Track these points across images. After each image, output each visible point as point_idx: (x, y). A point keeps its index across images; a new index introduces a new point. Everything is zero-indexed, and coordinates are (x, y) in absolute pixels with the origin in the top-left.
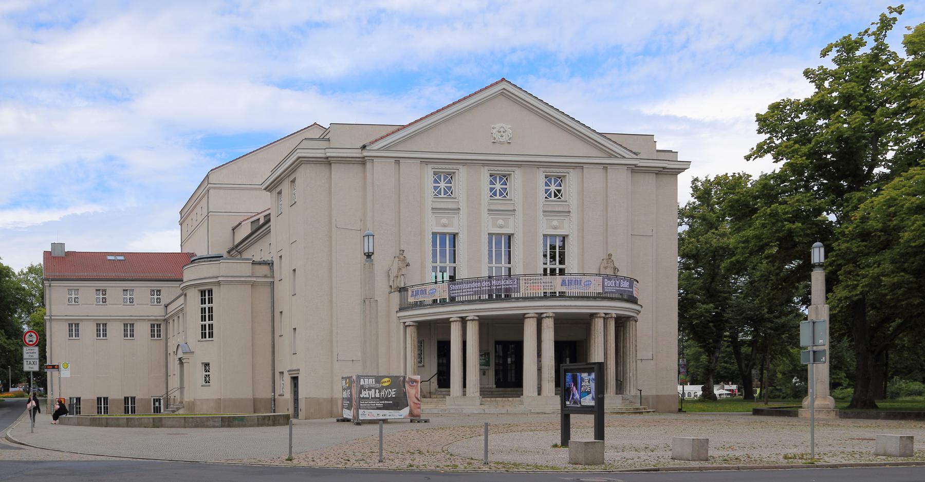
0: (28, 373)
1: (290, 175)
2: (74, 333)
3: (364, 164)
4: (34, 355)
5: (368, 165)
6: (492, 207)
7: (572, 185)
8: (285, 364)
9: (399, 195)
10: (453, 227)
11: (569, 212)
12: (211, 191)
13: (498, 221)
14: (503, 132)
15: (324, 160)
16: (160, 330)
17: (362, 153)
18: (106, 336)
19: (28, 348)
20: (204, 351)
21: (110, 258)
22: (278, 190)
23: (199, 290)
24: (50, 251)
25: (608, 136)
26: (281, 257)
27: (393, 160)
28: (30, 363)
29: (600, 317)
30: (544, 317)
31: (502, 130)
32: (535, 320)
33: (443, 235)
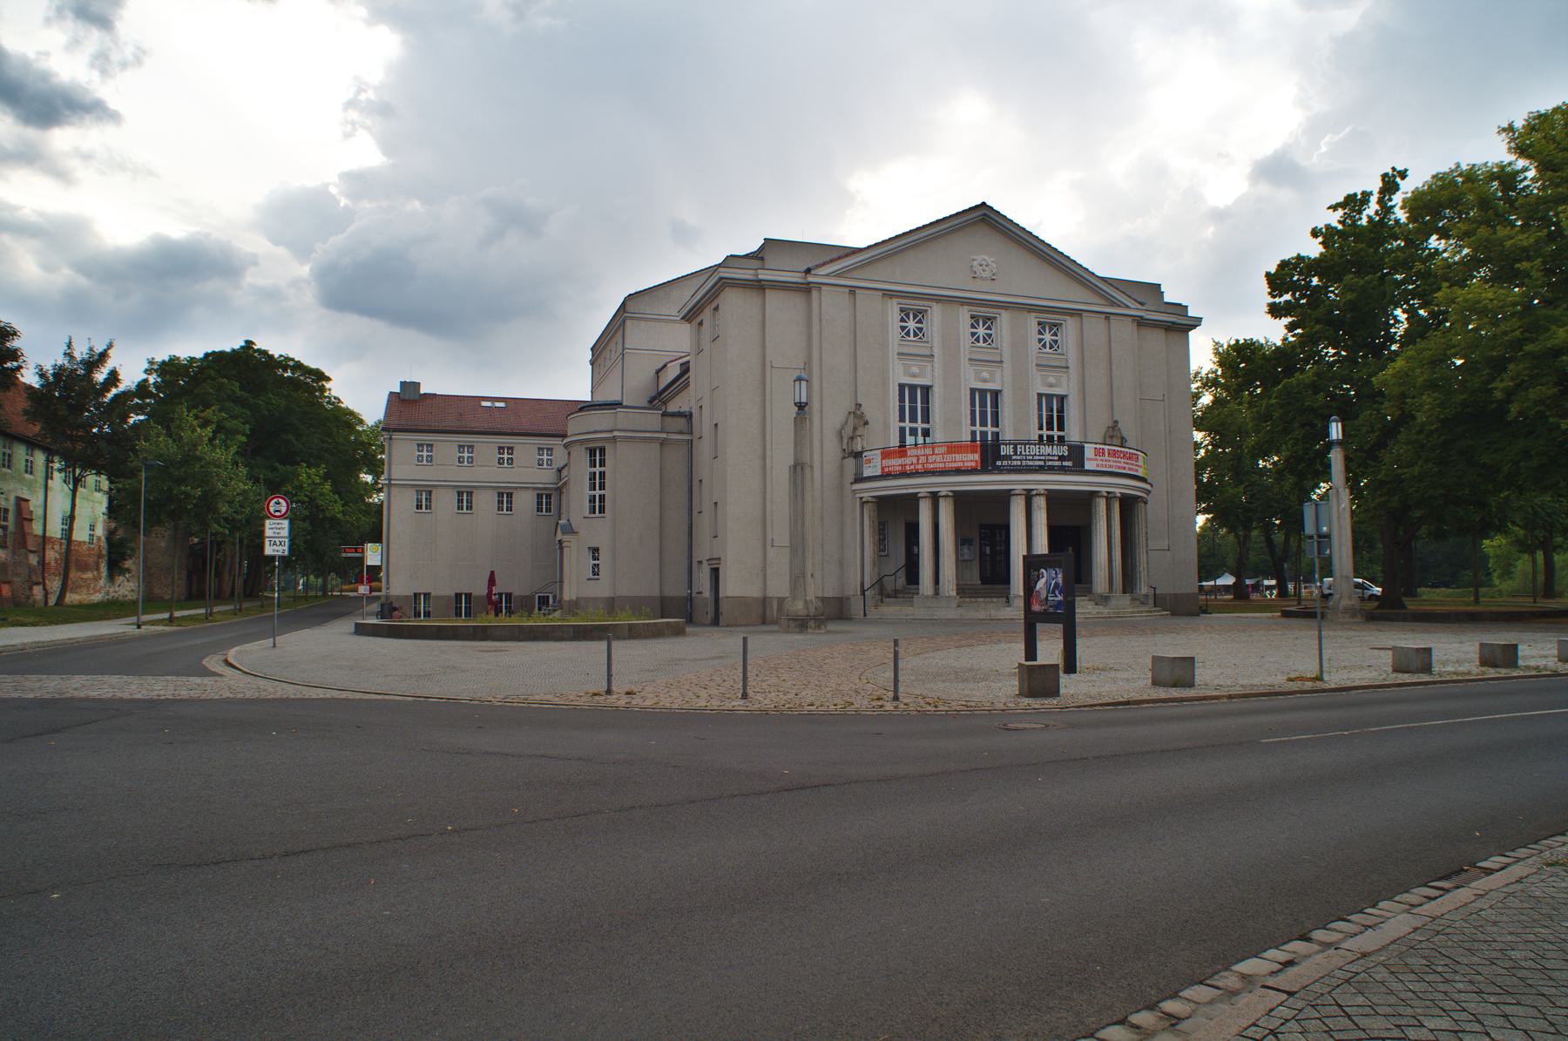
0: (273, 558)
2: (544, 507)
4: (281, 531)
5: (815, 294)
6: (974, 357)
8: (703, 552)
12: (629, 323)
15: (756, 284)
17: (806, 278)
19: (272, 521)
20: (596, 531)
21: (484, 404)
22: (698, 320)
24: (398, 391)
25: (1109, 281)
26: (701, 407)
28: (275, 544)
32: (1023, 497)
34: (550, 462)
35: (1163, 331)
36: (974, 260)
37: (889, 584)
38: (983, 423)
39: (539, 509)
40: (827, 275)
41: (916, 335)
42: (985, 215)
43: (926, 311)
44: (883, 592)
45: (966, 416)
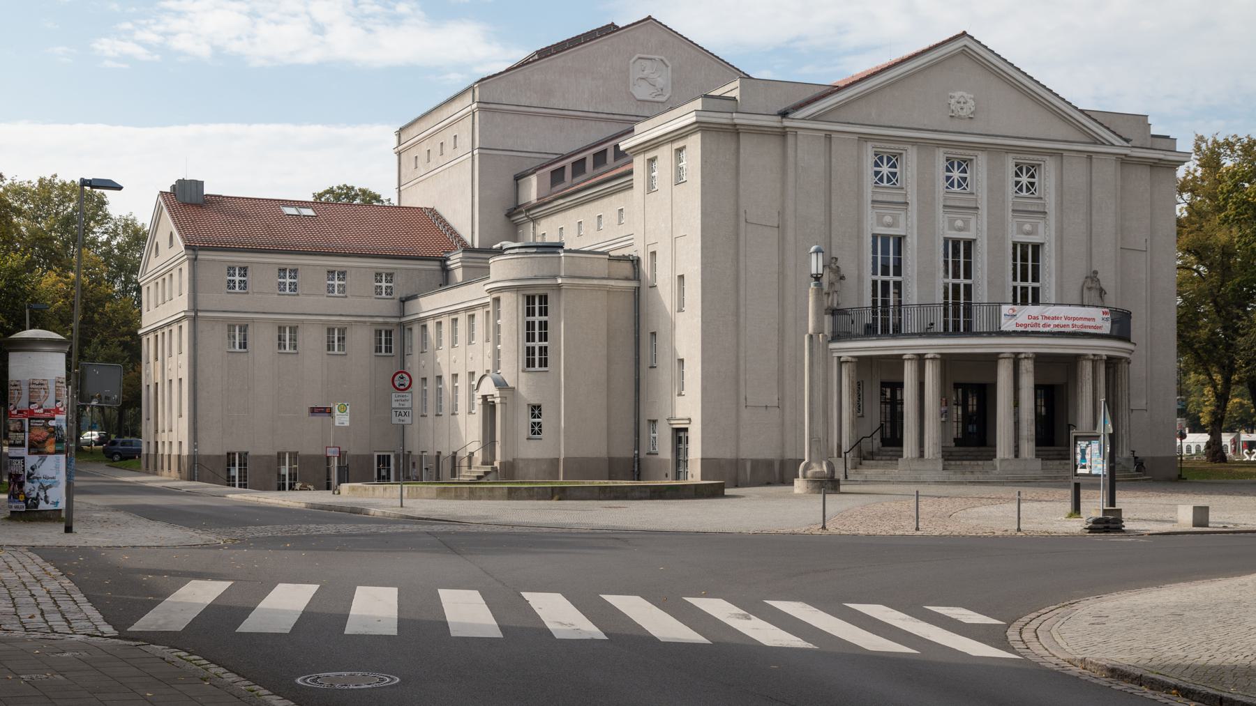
1: (675, 140)
3: (784, 136)
5: (790, 139)
6: (948, 203)
7: (1048, 178)
9: (830, 181)
10: (898, 227)
11: (1045, 213)
13: (956, 222)
14: (964, 103)
15: (731, 128)
16: (391, 340)
17: (782, 122)
18: (546, 366)
23: (524, 295)
25: (1086, 112)
27: (822, 134)
28: (400, 414)
29: (1089, 359)
30: (1022, 358)
31: (962, 100)
33: (885, 239)
34: (389, 291)
35: (1148, 169)
36: (951, 97)
37: (867, 446)
38: (956, 275)
39: (378, 349)
40: (803, 119)
41: (889, 180)
42: (965, 46)
43: (901, 154)
44: (863, 455)
45: (1222, 467)
